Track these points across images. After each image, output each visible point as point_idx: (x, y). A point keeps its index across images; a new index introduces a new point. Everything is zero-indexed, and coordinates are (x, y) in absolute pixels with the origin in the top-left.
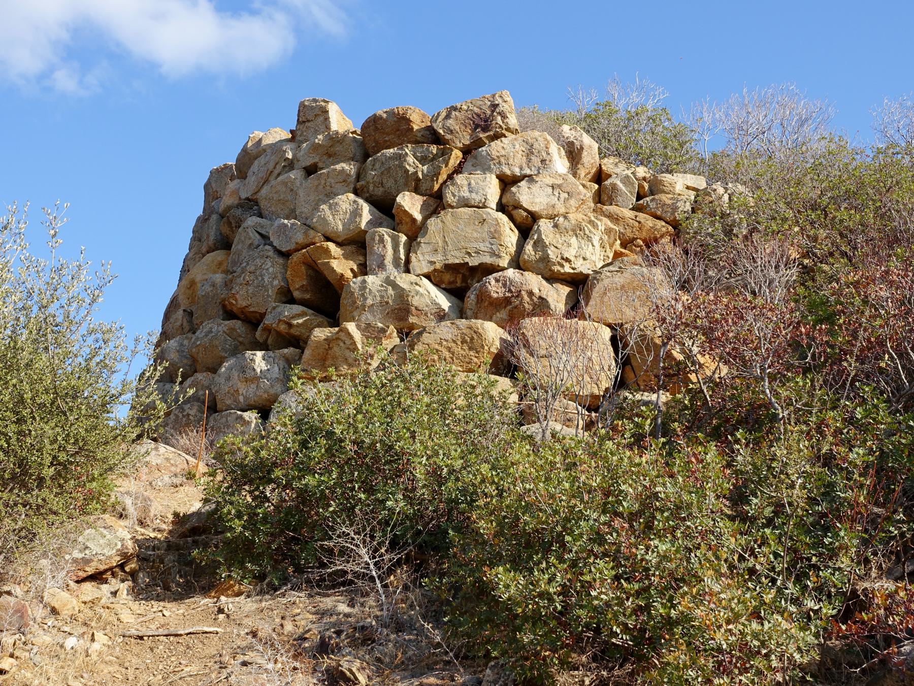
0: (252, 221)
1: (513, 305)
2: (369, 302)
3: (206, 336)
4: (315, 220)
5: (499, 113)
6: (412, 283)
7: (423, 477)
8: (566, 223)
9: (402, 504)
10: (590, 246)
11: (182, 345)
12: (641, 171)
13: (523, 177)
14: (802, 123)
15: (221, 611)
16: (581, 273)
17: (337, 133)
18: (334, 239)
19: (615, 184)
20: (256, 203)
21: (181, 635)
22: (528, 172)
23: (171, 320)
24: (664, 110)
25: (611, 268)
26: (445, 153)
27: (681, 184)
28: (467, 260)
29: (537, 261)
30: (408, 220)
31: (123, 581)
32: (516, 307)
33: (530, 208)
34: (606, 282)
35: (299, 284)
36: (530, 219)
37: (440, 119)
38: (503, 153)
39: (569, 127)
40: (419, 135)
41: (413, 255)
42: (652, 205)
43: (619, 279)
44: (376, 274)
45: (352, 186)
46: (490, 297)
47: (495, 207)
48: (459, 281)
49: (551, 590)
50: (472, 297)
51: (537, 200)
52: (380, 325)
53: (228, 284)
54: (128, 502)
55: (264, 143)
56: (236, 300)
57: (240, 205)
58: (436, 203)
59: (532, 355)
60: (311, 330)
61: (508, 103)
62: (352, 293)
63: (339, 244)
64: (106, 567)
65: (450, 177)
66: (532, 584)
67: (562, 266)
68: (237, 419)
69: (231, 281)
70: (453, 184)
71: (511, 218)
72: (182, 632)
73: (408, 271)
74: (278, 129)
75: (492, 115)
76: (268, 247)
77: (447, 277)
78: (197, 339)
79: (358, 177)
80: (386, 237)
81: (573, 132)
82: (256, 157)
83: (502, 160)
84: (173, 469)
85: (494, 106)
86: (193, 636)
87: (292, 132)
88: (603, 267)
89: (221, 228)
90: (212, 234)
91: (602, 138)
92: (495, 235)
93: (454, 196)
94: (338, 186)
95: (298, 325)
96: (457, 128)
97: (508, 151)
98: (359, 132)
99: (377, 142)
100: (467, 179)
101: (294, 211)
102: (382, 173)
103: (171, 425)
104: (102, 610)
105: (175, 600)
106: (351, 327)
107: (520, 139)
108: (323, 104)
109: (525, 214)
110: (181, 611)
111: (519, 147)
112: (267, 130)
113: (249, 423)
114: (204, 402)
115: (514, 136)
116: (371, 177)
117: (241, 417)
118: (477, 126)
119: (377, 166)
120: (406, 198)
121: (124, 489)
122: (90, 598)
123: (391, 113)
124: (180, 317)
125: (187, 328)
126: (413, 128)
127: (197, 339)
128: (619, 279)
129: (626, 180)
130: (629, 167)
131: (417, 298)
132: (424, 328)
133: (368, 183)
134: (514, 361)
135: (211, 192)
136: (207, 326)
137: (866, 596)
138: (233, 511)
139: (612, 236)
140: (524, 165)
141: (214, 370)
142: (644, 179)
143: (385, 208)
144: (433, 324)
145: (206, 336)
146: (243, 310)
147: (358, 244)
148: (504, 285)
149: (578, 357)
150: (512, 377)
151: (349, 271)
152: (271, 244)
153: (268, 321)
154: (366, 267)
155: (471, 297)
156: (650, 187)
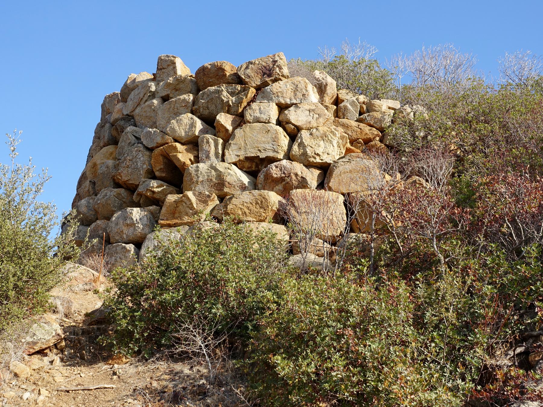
0: (130, 129)
1: (286, 181)
2: (201, 179)
3: (104, 198)
4: (168, 129)
5: (278, 66)
7: (233, 295)
8: (317, 133)
9: (221, 311)
10: (332, 146)
11: (89, 203)
12: (362, 98)
13: (292, 105)
14: (458, 67)
15: (114, 374)
16: (326, 162)
18: (179, 141)
19: (346, 106)
20: (133, 117)
21: (91, 390)
22: (295, 101)
23: (82, 187)
24: (375, 61)
25: (344, 160)
26: (245, 90)
27: (385, 106)
29: (300, 156)
31: (57, 354)
32: (288, 183)
33: (296, 124)
34: (341, 168)
37: (243, 69)
38: (280, 90)
39: (319, 72)
40: (230, 78)
42: (368, 119)
43: (348, 167)
44: (205, 162)
45: (190, 109)
46: (272, 177)
47: (275, 123)
48: (254, 167)
49: (309, 370)
50: (262, 176)
51: (300, 119)
53: (116, 167)
54: (58, 303)
55: (137, 81)
56: (121, 177)
57: (123, 119)
58: (240, 120)
60: (166, 195)
61: (283, 60)
62: (190, 174)
63: (183, 144)
64: (46, 346)
65: (249, 104)
66: (298, 366)
67: (315, 158)
68: (122, 248)
69: (118, 165)
70: (250, 109)
71: (285, 129)
72: (92, 388)
73: (223, 161)
74: (145, 73)
75: (273, 67)
76: (140, 145)
77: (247, 164)
78: (98, 199)
80: (210, 140)
81: (321, 75)
82: (133, 89)
83: (279, 94)
84: (84, 279)
85: (275, 62)
86: (98, 390)
87: (154, 74)
88: (339, 159)
89: (112, 131)
90: (106, 135)
91: (338, 77)
92: (275, 140)
93: (251, 115)
95: (159, 192)
97: (283, 89)
98: (194, 76)
99: (205, 83)
100: (259, 105)
102: (208, 101)
104: (44, 374)
105: (88, 366)
106: (190, 194)
107: (290, 82)
108: (172, 58)
109: (293, 127)
110: (91, 374)
111: (290, 87)
112: (139, 73)
113: (129, 251)
114: (102, 238)
115: (286, 80)
116: (201, 103)
117: (125, 247)
118: (264, 74)
119: (205, 97)
120: (222, 116)
121: (57, 295)
122: (37, 367)
123: (213, 65)
124: (88, 185)
127: (98, 199)
128: (348, 167)
129: (353, 104)
130: (354, 87)
131: (229, 177)
132: (233, 195)
133: (199, 107)
134: (286, 217)
135: (106, 110)
136: (104, 192)
137: (492, 368)
138: (121, 314)
139: (344, 140)
141: (108, 218)
142: (364, 103)
143: (210, 122)
144: (238, 193)
145: (104, 198)
146: (125, 183)
148: (281, 170)
149: (324, 214)
150: (286, 225)
152: (142, 143)
153: (140, 189)
154: (198, 158)
155: (261, 176)
156: (367, 108)
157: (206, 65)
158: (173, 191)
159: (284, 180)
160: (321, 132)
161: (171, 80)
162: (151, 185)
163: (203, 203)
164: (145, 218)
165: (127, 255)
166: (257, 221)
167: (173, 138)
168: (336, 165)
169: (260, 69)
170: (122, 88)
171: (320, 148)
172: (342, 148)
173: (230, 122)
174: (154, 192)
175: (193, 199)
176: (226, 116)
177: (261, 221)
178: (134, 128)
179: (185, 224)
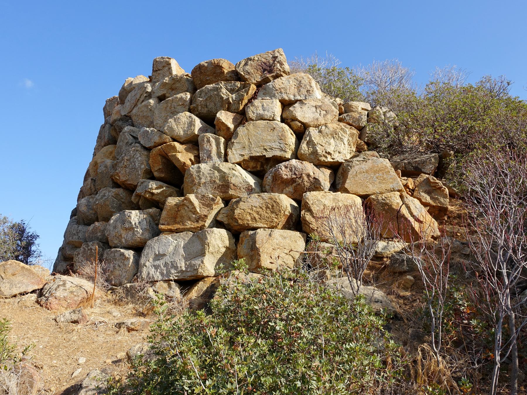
0: (127, 129)
1: (297, 183)
2: (203, 181)
3: (102, 198)
4: (166, 128)
5: (278, 62)
6: (230, 169)
8: (327, 130)
11: (89, 202)
13: (296, 101)
16: (338, 161)
17: (177, 76)
18: (178, 140)
20: (130, 117)
22: (299, 98)
25: (358, 159)
26: (246, 86)
28: (264, 154)
29: (309, 155)
32: (299, 184)
34: (357, 168)
35: (157, 168)
36: (302, 127)
37: (241, 66)
38: (283, 86)
40: (228, 76)
42: (348, 118)
44: (206, 163)
45: (187, 107)
46: (282, 178)
48: (259, 166)
50: (270, 177)
51: (307, 116)
52: (211, 196)
53: (114, 166)
55: (133, 83)
56: (119, 177)
57: (121, 119)
58: (242, 118)
59: (313, 217)
61: (282, 58)
62: (192, 175)
63: (182, 143)
65: (250, 101)
69: (116, 164)
70: (252, 106)
73: (226, 160)
74: (141, 76)
76: (137, 145)
77: (252, 164)
78: (97, 200)
79: (191, 100)
80: (211, 139)
82: (130, 91)
83: (282, 90)
84: (76, 298)
85: (275, 58)
87: (150, 77)
89: (110, 136)
92: (282, 138)
93: (254, 113)
94: (179, 107)
95: (158, 194)
96: (252, 71)
97: (286, 85)
98: (190, 75)
99: (201, 81)
101: (152, 122)
103: (81, 255)
106: (192, 197)
107: (293, 78)
108: (168, 60)
109: (300, 124)
112: (135, 76)
113: (128, 259)
117: (123, 254)
118: (265, 70)
119: (203, 95)
120: (223, 114)
123: (210, 63)
124: (90, 183)
125: (93, 190)
126: (224, 72)
127: (97, 200)
128: (365, 166)
133: (197, 105)
135: (107, 113)
140: (296, 94)
141: (107, 219)
142: (340, 104)
143: (210, 121)
145: (102, 198)
147: (193, 143)
148: (291, 170)
152: (139, 143)
153: (139, 190)
154: (199, 158)
155: (269, 178)
157: (203, 63)
158: (173, 192)
159: (295, 182)
160: (331, 129)
161: (167, 80)
162: (150, 187)
163: (207, 206)
164: (145, 222)
165: (126, 263)
166: (269, 228)
167: (171, 137)
169: (259, 65)
172: (352, 147)
173: (231, 120)
174: (153, 194)
176: (227, 114)
177: (273, 227)
178: (132, 128)
179: (189, 230)
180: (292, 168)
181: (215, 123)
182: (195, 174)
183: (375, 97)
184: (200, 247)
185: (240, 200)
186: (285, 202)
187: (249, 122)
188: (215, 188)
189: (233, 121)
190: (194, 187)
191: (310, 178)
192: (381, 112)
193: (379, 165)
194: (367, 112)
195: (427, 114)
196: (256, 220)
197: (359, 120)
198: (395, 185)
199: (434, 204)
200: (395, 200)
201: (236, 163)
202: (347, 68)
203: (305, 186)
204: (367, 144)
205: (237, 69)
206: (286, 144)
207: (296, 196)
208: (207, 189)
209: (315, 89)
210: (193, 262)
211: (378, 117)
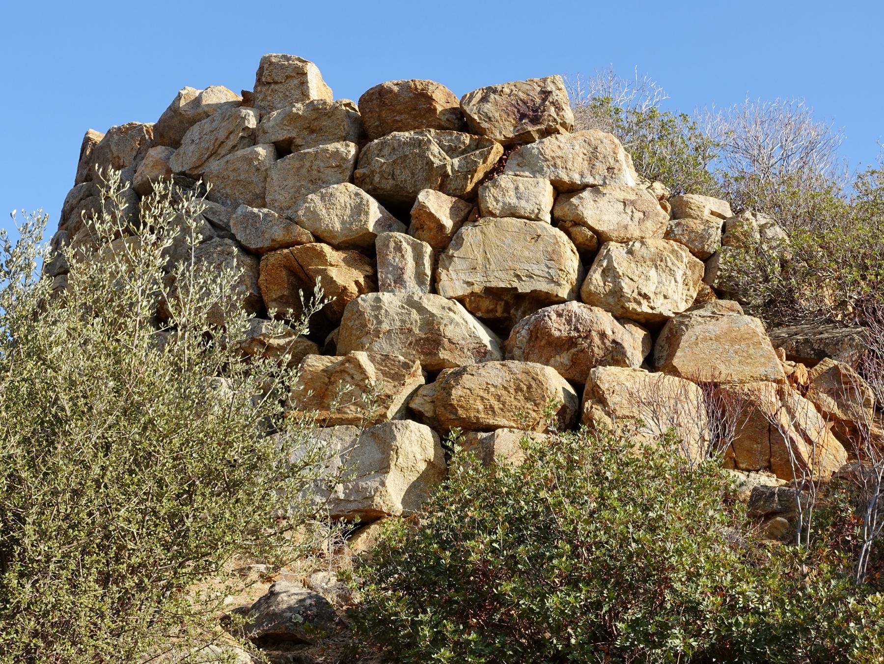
2: (385, 326)
4: (301, 213)
5: (552, 103)
6: (443, 308)
8: (644, 249)
10: (673, 281)
13: (584, 187)
16: (661, 314)
17: (325, 103)
18: (327, 239)
22: (590, 180)
25: (701, 312)
28: (515, 285)
29: (605, 295)
30: (432, 225)
32: (582, 351)
34: (698, 329)
36: (595, 240)
37: (475, 101)
38: (560, 153)
40: (444, 118)
41: (443, 274)
44: (392, 291)
45: (348, 173)
46: (550, 335)
47: (549, 221)
50: (523, 332)
51: (605, 218)
52: (401, 358)
55: (204, 103)
58: (471, 208)
59: (608, 414)
61: (561, 96)
62: (361, 314)
63: (336, 248)
65: (489, 176)
67: (639, 304)
70: (495, 186)
73: (434, 290)
74: (222, 88)
77: (486, 304)
79: (357, 158)
80: (404, 245)
82: (192, 122)
83: (559, 162)
85: (546, 94)
87: (244, 93)
92: (553, 256)
93: (497, 201)
96: (497, 115)
97: (566, 152)
99: (383, 122)
100: (513, 181)
106: (362, 357)
107: (581, 139)
108: (300, 64)
109: (590, 233)
118: (523, 116)
119: (386, 151)
120: (431, 197)
123: (405, 87)
126: (435, 109)
131: (451, 327)
133: (373, 172)
140: (586, 172)
143: (401, 209)
148: (569, 322)
151: (353, 284)
155: (521, 333)
157: (388, 84)
158: (310, 347)
160: (653, 250)
161: (299, 108)
163: (393, 379)
167: (312, 233)
168: (686, 320)
170: (164, 114)
171: (650, 283)
172: (691, 288)
173: (448, 211)
175: (370, 368)
179: (354, 422)
180: (570, 317)
181: (412, 212)
182: (368, 312)
183: (742, 188)
184: (378, 456)
185: (460, 372)
186: (554, 381)
187: (487, 219)
188: (410, 344)
189: (451, 213)
190: (364, 334)
191: (606, 341)
192: (754, 224)
193: (742, 329)
194: (721, 222)
195: (846, 242)
196: (494, 412)
197: (703, 237)
198: (769, 370)
199: (845, 418)
200: (768, 397)
201: (455, 298)
202: (684, 117)
203: (593, 356)
204: (721, 289)
205: (465, 107)
206: (561, 270)
207: (575, 374)
208: (391, 345)
209: (624, 166)
210: (362, 484)
211: (746, 234)
